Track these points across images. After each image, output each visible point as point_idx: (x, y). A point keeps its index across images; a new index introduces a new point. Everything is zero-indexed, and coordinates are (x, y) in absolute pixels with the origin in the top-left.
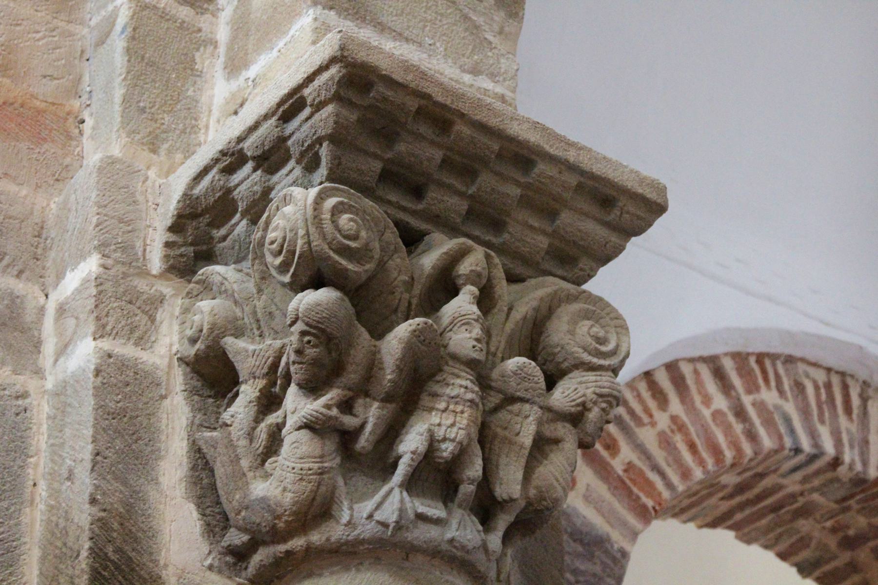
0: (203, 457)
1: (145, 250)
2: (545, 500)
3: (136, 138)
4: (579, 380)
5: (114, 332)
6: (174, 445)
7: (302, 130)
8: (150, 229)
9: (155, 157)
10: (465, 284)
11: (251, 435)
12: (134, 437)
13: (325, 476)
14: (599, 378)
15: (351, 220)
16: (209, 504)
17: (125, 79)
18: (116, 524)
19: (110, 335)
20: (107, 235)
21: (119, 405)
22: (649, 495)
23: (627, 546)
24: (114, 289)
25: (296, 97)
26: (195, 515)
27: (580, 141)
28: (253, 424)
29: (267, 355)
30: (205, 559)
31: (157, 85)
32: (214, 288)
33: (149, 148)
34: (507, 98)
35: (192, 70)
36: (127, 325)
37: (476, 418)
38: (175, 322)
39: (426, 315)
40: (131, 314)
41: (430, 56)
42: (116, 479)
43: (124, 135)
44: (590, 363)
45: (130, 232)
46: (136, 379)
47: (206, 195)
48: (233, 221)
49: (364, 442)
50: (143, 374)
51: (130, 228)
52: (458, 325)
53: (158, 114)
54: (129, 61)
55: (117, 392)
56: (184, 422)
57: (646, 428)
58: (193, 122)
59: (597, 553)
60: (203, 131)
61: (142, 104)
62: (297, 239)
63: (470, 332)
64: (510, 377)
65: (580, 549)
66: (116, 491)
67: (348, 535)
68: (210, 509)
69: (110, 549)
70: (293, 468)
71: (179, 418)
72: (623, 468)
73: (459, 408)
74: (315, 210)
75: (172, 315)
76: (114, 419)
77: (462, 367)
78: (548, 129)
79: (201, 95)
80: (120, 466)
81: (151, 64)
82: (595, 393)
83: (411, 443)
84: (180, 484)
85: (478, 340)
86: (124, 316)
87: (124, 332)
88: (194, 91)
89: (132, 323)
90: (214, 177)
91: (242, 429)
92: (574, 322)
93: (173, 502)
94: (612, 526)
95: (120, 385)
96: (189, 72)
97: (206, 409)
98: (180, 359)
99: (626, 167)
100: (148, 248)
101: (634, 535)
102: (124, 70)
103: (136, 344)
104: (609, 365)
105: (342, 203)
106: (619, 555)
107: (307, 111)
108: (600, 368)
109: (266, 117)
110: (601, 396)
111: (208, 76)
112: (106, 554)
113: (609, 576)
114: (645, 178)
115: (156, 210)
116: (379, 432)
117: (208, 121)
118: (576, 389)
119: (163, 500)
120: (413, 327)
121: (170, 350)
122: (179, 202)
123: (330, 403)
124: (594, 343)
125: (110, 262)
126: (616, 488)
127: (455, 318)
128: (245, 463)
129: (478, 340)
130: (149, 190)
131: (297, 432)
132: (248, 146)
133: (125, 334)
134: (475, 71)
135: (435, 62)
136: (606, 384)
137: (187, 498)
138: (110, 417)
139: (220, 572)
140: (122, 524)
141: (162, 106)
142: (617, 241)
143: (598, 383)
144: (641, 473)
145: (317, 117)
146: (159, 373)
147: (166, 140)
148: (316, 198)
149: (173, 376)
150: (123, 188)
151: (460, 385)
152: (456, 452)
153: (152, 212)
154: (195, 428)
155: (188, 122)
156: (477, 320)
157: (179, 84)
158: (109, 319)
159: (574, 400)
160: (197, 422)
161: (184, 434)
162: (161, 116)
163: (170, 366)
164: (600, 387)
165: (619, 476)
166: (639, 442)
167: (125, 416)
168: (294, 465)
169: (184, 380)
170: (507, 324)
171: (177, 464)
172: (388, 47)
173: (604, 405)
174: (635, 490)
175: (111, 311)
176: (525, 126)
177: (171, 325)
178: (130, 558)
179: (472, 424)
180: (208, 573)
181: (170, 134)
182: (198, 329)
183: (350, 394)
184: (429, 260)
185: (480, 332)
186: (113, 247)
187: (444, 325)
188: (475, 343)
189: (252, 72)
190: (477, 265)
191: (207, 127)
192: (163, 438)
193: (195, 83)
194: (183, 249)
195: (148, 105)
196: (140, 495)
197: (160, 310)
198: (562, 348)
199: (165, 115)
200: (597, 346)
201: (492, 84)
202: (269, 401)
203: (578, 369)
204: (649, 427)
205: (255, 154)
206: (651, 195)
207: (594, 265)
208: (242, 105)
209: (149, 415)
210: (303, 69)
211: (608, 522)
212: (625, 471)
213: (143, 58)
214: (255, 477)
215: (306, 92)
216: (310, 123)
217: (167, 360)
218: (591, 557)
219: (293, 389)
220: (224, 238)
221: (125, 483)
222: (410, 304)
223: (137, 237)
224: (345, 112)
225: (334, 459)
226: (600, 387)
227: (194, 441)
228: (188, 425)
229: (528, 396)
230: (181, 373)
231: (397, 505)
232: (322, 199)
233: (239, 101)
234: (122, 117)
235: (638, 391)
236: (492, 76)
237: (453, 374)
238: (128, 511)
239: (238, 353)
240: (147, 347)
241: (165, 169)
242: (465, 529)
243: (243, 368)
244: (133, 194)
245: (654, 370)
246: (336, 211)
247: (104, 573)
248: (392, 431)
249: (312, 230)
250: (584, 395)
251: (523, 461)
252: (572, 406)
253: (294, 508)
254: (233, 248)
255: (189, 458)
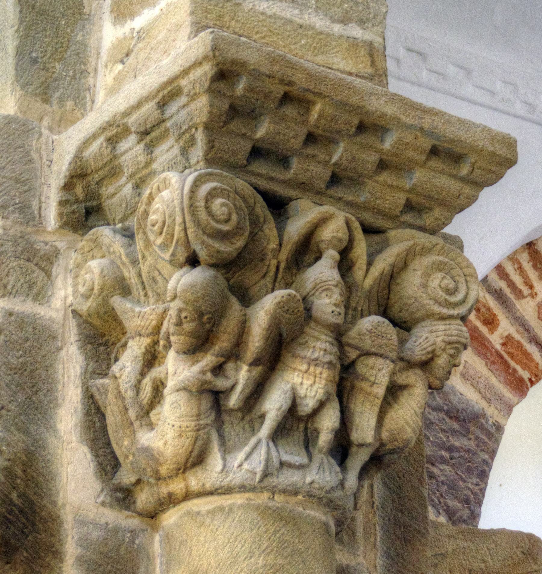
0: (95, 403)
1: (40, 208)
2: (397, 440)
3: (30, 90)
4: (430, 329)
5: (15, 290)
6: (70, 393)
7: (180, 115)
8: (45, 186)
9: (47, 107)
10: (328, 248)
11: (137, 387)
12: (34, 390)
13: (201, 432)
14: (448, 327)
15: (223, 205)
16: (101, 445)
17: (17, 31)
18: (19, 471)
19: (10, 294)
20: (5, 197)
21: (21, 360)
22: (525, 367)
23: (501, 421)
24: (13, 249)
25: (173, 85)
26: (89, 456)
27: (435, 107)
28: (139, 377)
29: (151, 317)
30: (99, 496)
31: (48, 33)
32: (104, 248)
33: (42, 99)
34: (376, 45)
35: (80, 14)
36: (25, 282)
37: (334, 377)
38: (69, 275)
39: (288, 285)
40: (30, 271)
41: (301, 11)
42: (18, 430)
43: (18, 88)
44: (440, 313)
45: (26, 191)
46: (35, 334)
47: (95, 158)
48: (120, 183)
49: (234, 400)
50: (41, 328)
51: (26, 188)
52: (320, 290)
53: (49, 63)
54: (21, 12)
55: (18, 348)
56: (78, 370)
57: (525, 301)
58: (83, 67)
59: (472, 428)
60: (92, 75)
61: (34, 55)
62: (175, 225)
63: (330, 297)
64: (365, 335)
65: (456, 426)
66: (19, 441)
67: (221, 482)
68: (102, 450)
69: (14, 496)
70: (173, 426)
71: (74, 367)
72: (501, 341)
73: (319, 370)
74: (191, 198)
75: (66, 269)
76: (15, 373)
77: (322, 330)
78: (405, 99)
79: (89, 39)
80: (22, 417)
81: (42, 13)
82: (444, 341)
83: (274, 404)
84: (75, 430)
85: (336, 305)
86: (22, 274)
87: (22, 290)
88: (83, 35)
89: (30, 280)
90: (102, 144)
91: (130, 381)
92: (427, 275)
93: (70, 446)
94: (489, 401)
95: (21, 341)
96: (78, 16)
97: (98, 357)
98: (74, 312)
99: (478, 126)
100: (43, 205)
101: (509, 409)
102: (16, 21)
103: (35, 300)
104: (458, 315)
105: (215, 189)
106: (493, 430)
107: (183, 99)
108: (450, 317)
109: (147, 99)
110: (450, 343)
111: (96, 18)
112: (11, 500)
113: (483, 450)
114: (497, 134)
115: (49, 166)
116: (248, 390)
117: (97, 63)
118: (427, 339)
119: (60, 445)
120: (279, 299)
121: (65, 303)
122: (70, 163)
123: (205, 369)
124: (444, 295)
125: (9, 223)
126: (493, 363)
127: (317, 284)
128: (132, 414)
129: (336, 305)
130: (43, 147)
131: (176, 394)
132: (132, 120)
133: (24, 292)
134: (344, 21)
135: (306, 16)
136: (454, 332)
137: (82, 442)
138: (12, 373)
139: (111, 506)
140: (24, 471)
141: (53, 54)
142: (471, 192)
143: (448, 332)
144: (519, 346)
145: (193, 106)
146: (56, 326)
147: (57, 88)
148: (192, 187)
149: (67, 329)
150: (20, 147)
151: (318, 346)
152: (315, 407)
153: (46, 168)
154: (88, 376)
155: (77, 67)
156: (336, 286)
157: (69, 31)
158: (10, 278)
159: (425, 349)
160: (90, 369)
161: (78, 382)
162: (52, 65)
163: (65, 319)
164: (448, 335)
165: (497, 351)
166: (518, 314)
167: (25, 370)
168: (173, 423)
169: (78, 330)
170: (366, 280)
171: (72, 411)
172: (262, 8)
173: (452, 352)
174: (513, 364)
175: (11, 270)
176: (383, 100)
177: (65, 278)
178: (32, 501)
179: (329, 383)
180: (101, 509)
181: (61, 82)
182: (90, 288)
183: (223, 359)
184: (296, 228)
185: (339, 298)
186: (11, 209)
187: (307, 290)
188: (334, 308)
189: (139, 22)
190: (338, 232)
191: (96, 70)
192: (60, 387)
193: (84, 27)
194: (75, 206)
195: (40, 55)
196: (41, 443)
197: (56, 265)
198: (415, 300)
199: (57, 64)
200: (447, 297)
201: (361, 31)
202: (151, 359)
203: (429, 319)
204: (529, 298)
205: (138, 130)
206: (501, 151)
207: (449, 214)
208: (127, 55)
209: (47, 366)
210: (180, 62)
211: (484, 398)
212: (504, 344)
213: (33, 8)
214: (141, 426)
215: (184, 82)
216: (187, 109)
217: (63, 312)
218: (466, 433)
219: (172, 354)
220: (113, 195)
221: (26, 432)
222: (278, 268)
223: (33, 195)
224: (217, 102)
225: (210, 415)
226: (448, 335)
227: (87, 388)
228: (81, 373)
229: (382, 351)
230: (75, 324)
231: (263, 457)
232: (196, 186)
233: (125, 51)
234: (16, 70)
235: (519, 263)
236: (361, 23)
237: (314, 337)
238: (29, 458)
239: (124, 312)
240: (44, 301)
241: (57, 118)
242: (324, 473)
243: (131, 324)
244: (28, 153)
245: (537, 240)
246: (210, 196)
247: (9, 517)
248: (258, 391)
249: (188, 218)
250: (435, 344)
251: (376, 409)
252: (423, 355)
253: (175, 459)
254: (121, 206)
255: (83, 404)
